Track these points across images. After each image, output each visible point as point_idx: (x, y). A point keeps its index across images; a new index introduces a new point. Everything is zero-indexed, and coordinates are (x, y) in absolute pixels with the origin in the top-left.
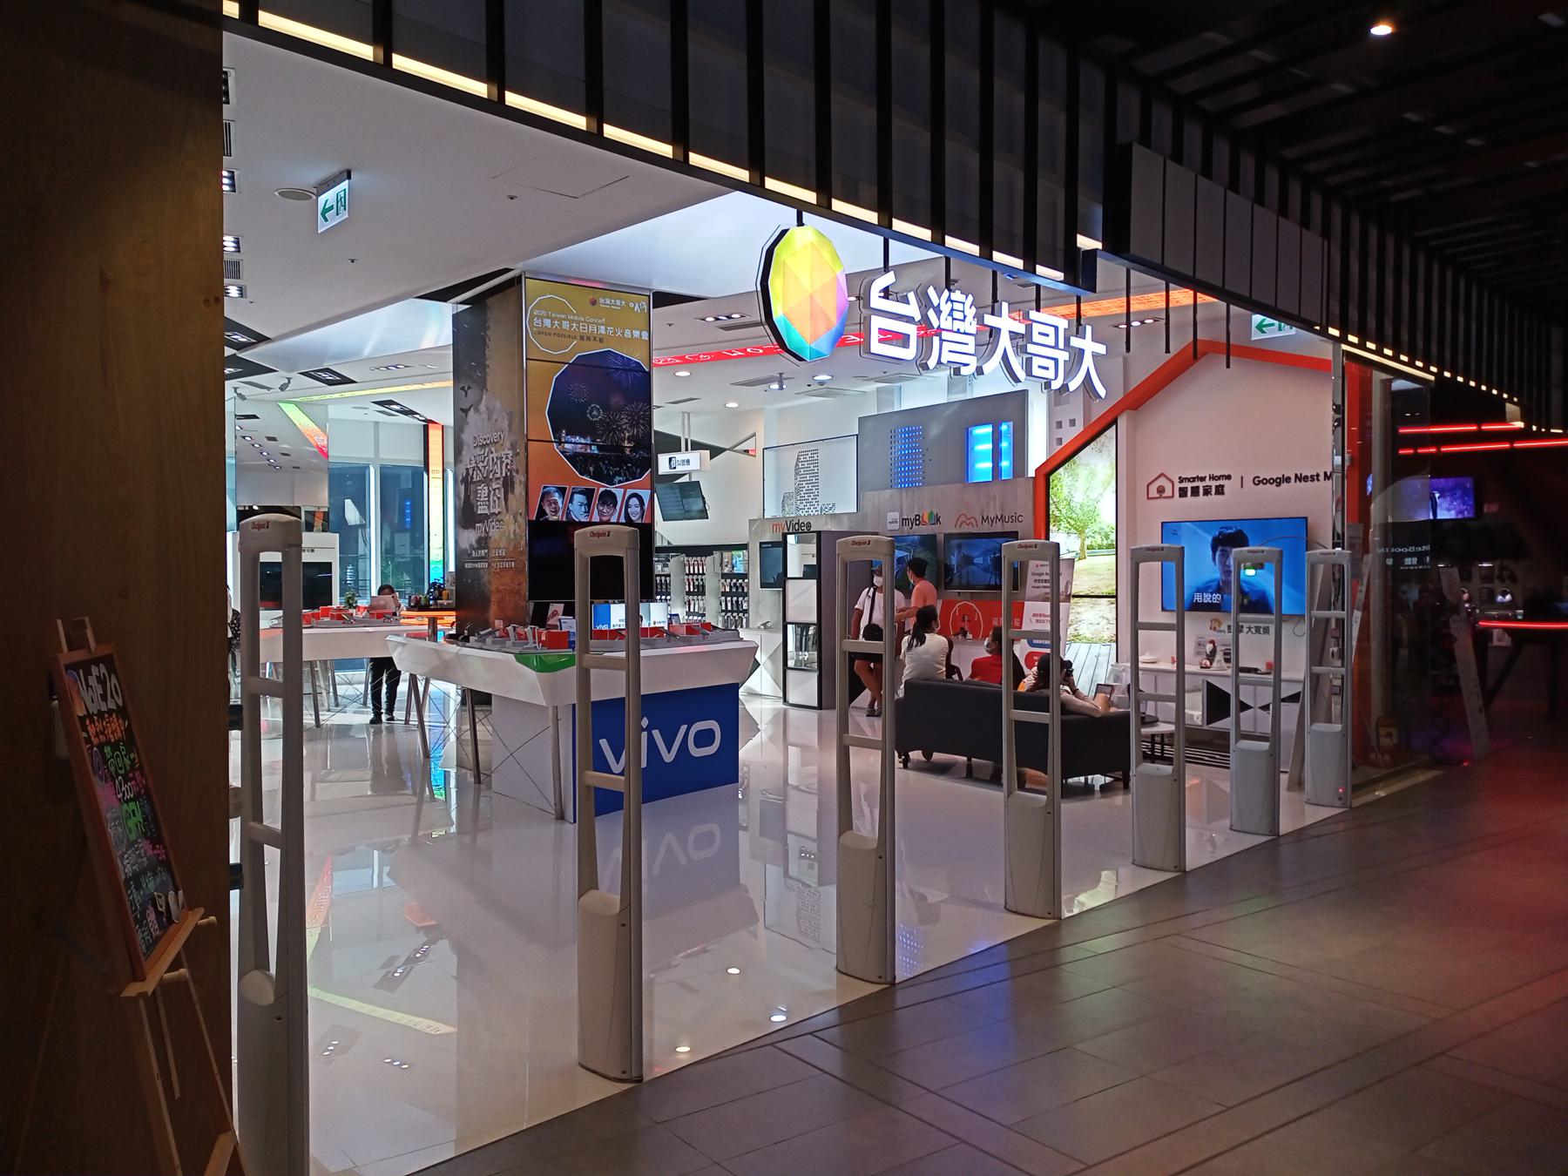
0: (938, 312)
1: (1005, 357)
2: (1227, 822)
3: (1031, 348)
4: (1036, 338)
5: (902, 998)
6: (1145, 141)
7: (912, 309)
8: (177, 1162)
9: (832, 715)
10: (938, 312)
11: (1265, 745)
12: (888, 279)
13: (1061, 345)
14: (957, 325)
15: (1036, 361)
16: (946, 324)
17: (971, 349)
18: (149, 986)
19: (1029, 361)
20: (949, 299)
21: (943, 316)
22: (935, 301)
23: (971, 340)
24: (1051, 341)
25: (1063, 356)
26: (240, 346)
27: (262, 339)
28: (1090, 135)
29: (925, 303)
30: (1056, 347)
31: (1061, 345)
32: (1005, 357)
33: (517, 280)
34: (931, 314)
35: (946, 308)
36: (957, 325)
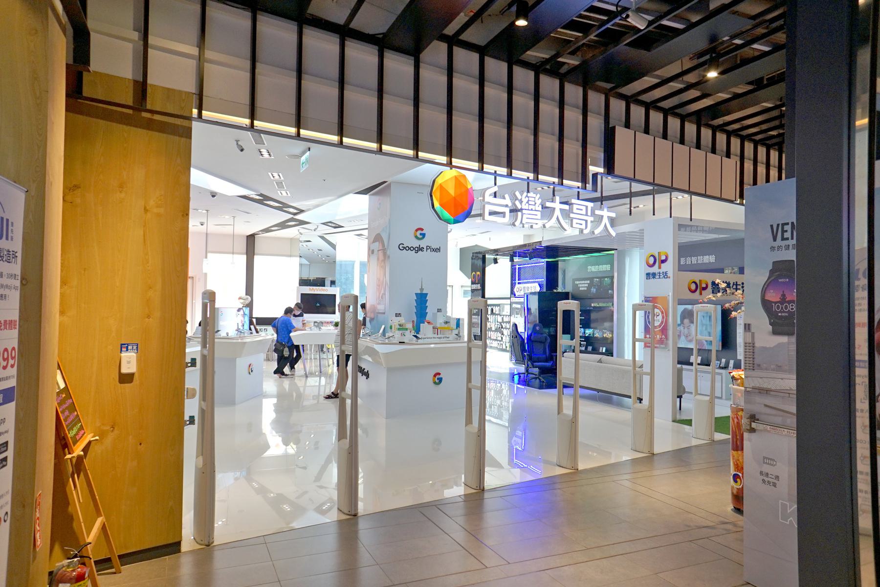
0: (521, 201)
1: (558, 218)
2: (268, 453)
3: (572, 215)
4: (575, 211)
5: (486, 495)
6: (627, 125)
7: (508, 201)
8: (865, 522)
9: (649, 350)
10: (521, 201)
11: (707, 398)
12: (496, 189)
13: (589, 214)
14: (531, 207)
15: (575, 221)
16: (526, 207)
17: (539, 217)
18: (75, 455)
19: (572, 221)
20: (527, 196)
21: (523, 204)
22: (519, 197)
23: (539, 214)
24: (584, 212)
25: (590, 219)
26: (295, 214)
27: (302, 211)
28: (596, 124)
29: (514, 198)
30: (587, 215)
31: (589, 214)
32: (558, 218)
33: (390, 185)
34: (517, 203)
35: (525, 200)
36: (531, 207)
